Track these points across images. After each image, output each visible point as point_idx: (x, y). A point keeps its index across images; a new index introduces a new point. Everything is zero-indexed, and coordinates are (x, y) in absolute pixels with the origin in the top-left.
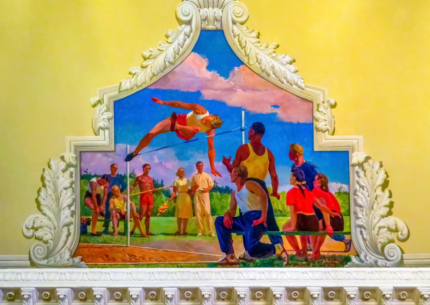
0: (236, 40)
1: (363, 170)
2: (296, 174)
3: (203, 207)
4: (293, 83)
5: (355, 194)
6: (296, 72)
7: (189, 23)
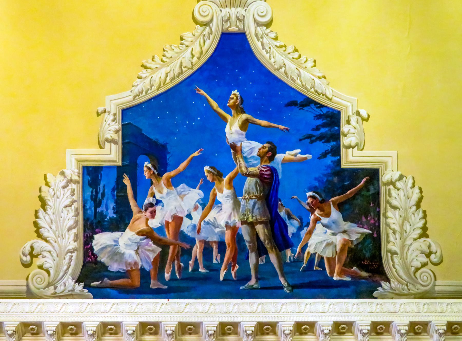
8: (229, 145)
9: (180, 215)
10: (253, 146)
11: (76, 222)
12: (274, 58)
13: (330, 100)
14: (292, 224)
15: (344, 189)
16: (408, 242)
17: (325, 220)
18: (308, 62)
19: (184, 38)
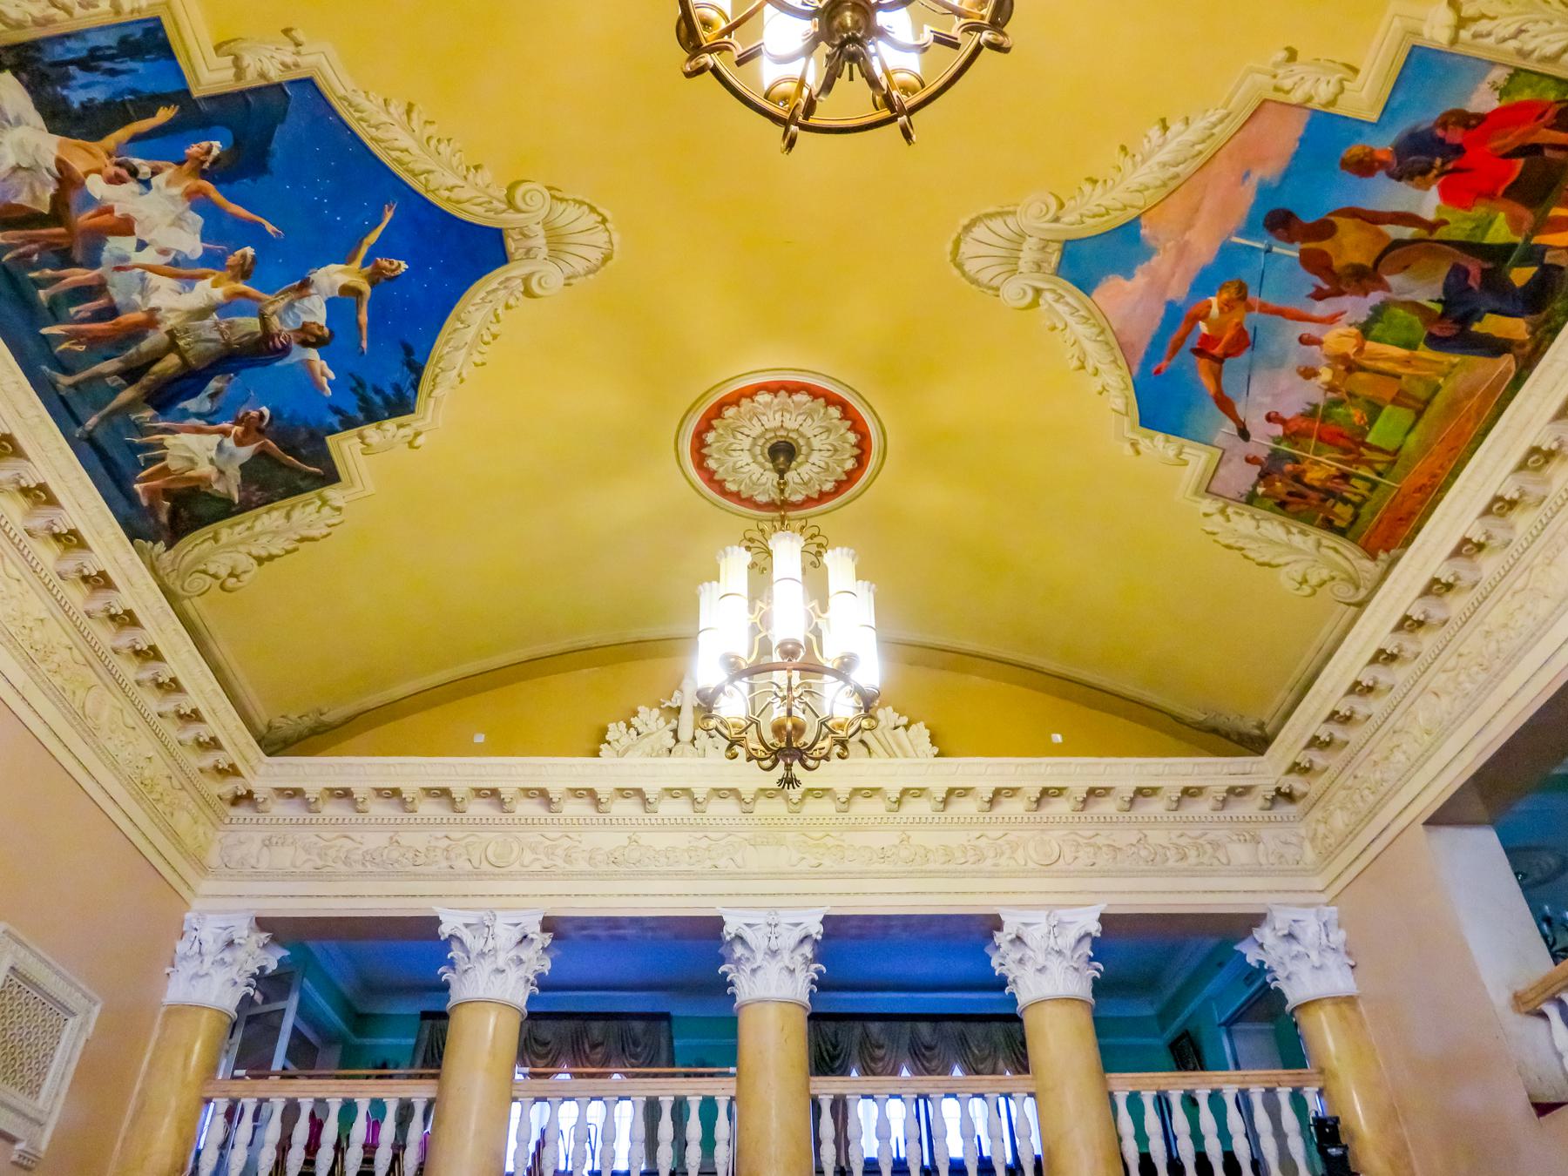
0: (1089, 221)
1: (1474, 20)
2: (1410, 173)
3: (1390, 359)
4: (1208, 132)
5: (1525, 55)
6: (1187, 121)
7: (1038, 292)
8: (307, 276)
9: (137, 229)
10: (318, 313)
11: (20, 25)
12: (477, 310)
13: (429, 396)
14: (201, 402)
15: (291, 450)
16: (242, 548)
17: (229, 443)
18: (481, 356)
19: (479, 171)
